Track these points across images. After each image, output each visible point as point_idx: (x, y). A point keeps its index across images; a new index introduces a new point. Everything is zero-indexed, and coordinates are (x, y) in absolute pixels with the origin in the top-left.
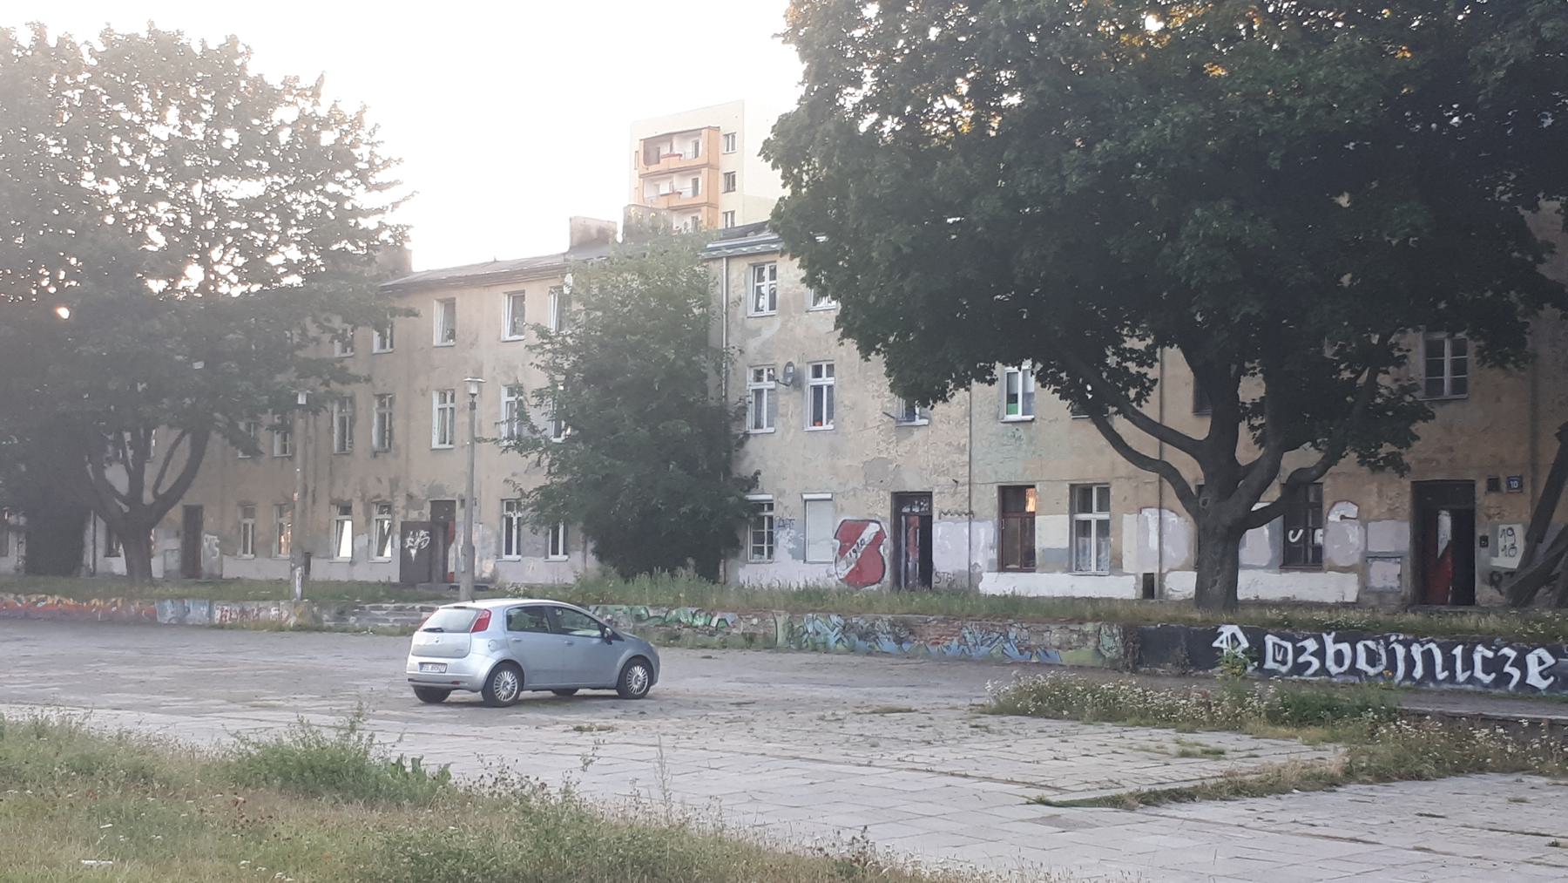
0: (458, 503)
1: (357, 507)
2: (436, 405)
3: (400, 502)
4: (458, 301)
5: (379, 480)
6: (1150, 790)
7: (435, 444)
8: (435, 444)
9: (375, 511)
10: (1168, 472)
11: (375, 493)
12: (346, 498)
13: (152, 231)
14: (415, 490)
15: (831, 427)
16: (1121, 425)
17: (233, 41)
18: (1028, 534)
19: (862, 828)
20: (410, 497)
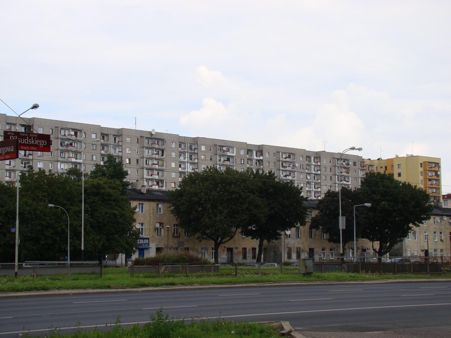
0: (367, 249)
11: (351, 247)
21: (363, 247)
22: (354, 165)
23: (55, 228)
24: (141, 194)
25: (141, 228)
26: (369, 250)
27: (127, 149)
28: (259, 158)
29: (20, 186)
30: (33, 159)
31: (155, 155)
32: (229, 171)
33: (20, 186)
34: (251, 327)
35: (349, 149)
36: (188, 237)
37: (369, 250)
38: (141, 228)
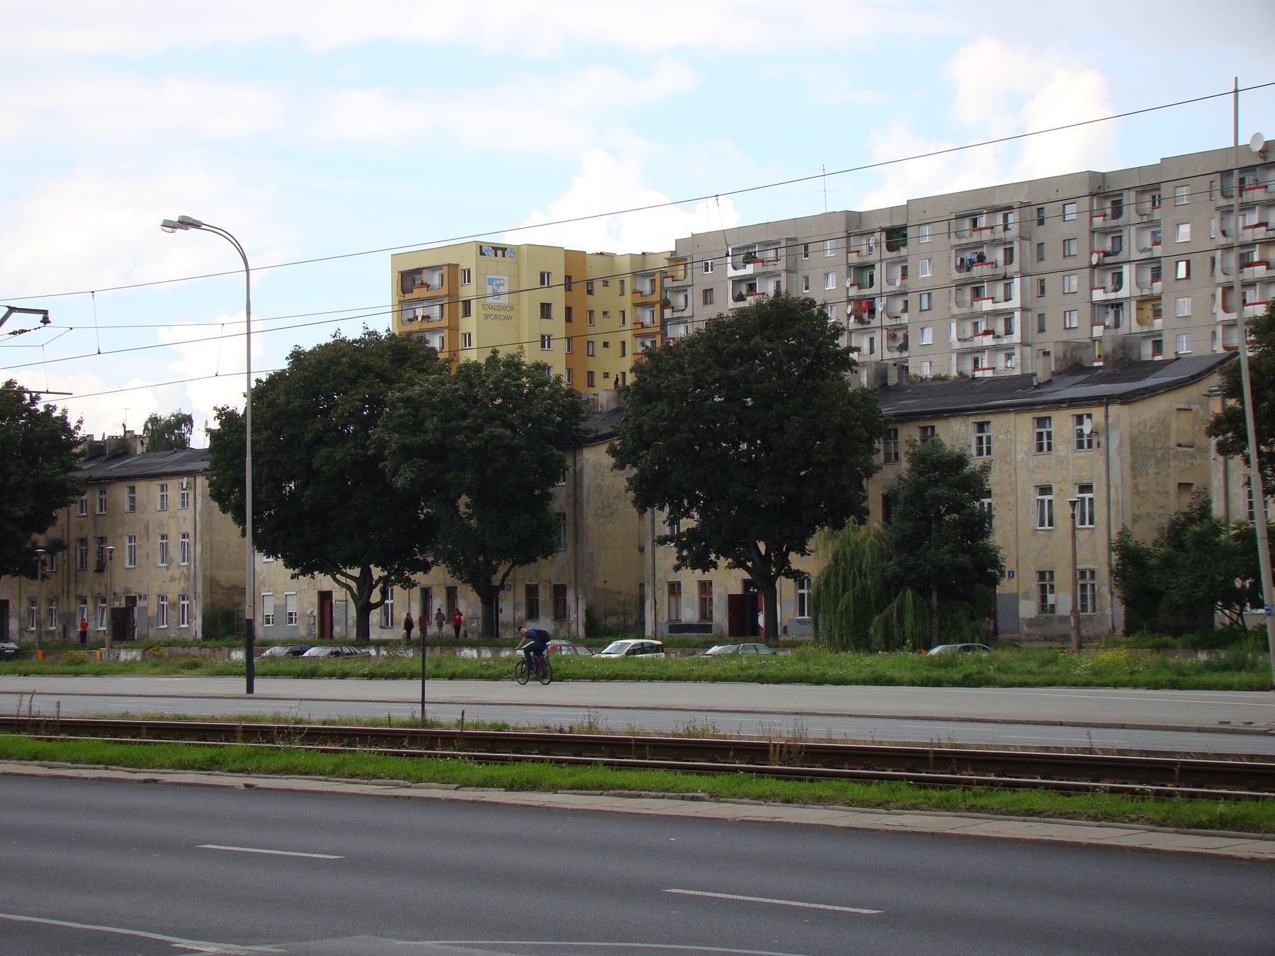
0: (138, 598)
1: (90, 600)
2: (127, 544)
3: (110, 597)
4: (899, 430)
5: (100, 585)
6: (291, 742)
7: (127, 565)
8: (127, 565)
9: (99, 602)
10: (349, 588)
11: (98, 592)
12: (84, 595)
13: (1270, 473)
14: (117, 591)
15: (564, 483)
16: (338, 576)
17: (1159, 530)
18: (366, 594)
19: (1010, 226)
20: (115, 594)
21: (127, 590)
22: (543, 317)
23: (823, 451)
24: (1167, 364)
25: (1083, 448)
26: (145, 599)
27: (1074, 217)
28: (741, 272)
29: (47, 407)
30: (1087, 265)
31: (1250, 230)
32: (301, 360)
33: (47, 407)
34: (49, 654)
35: (203, 227)
36: (635, 502)
37: (145, 599)
38: (1083, 448)
